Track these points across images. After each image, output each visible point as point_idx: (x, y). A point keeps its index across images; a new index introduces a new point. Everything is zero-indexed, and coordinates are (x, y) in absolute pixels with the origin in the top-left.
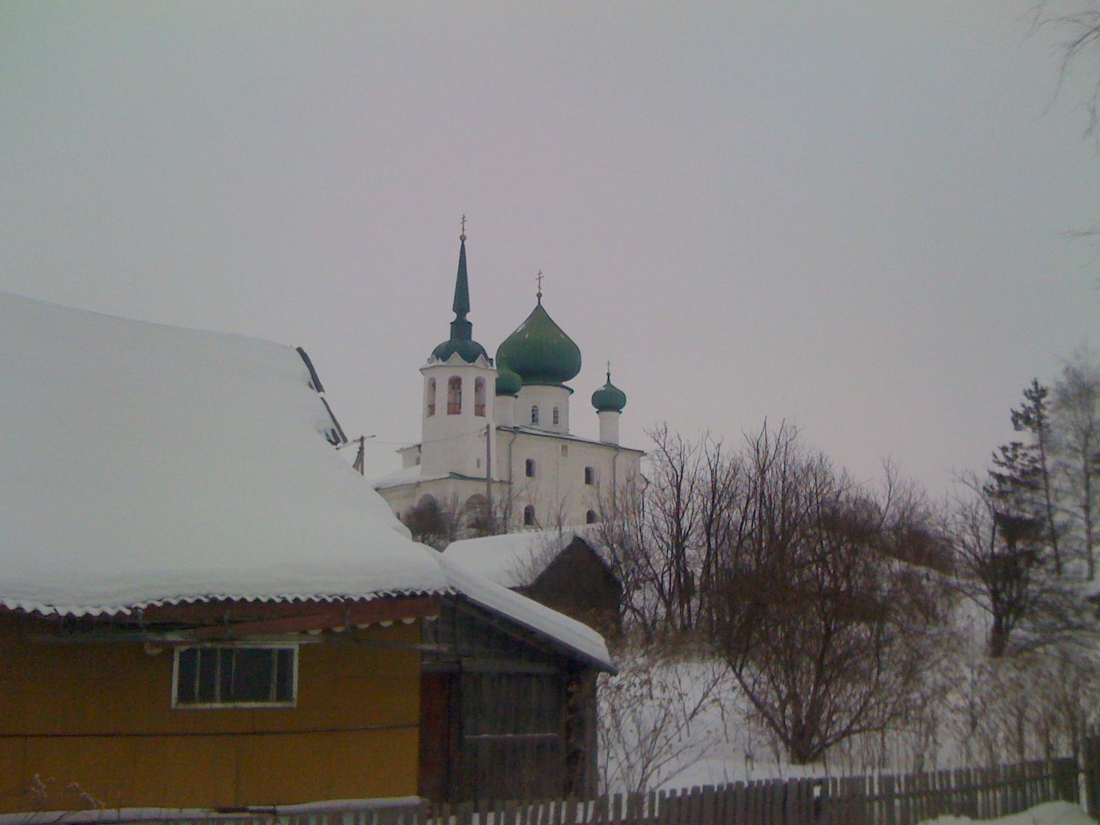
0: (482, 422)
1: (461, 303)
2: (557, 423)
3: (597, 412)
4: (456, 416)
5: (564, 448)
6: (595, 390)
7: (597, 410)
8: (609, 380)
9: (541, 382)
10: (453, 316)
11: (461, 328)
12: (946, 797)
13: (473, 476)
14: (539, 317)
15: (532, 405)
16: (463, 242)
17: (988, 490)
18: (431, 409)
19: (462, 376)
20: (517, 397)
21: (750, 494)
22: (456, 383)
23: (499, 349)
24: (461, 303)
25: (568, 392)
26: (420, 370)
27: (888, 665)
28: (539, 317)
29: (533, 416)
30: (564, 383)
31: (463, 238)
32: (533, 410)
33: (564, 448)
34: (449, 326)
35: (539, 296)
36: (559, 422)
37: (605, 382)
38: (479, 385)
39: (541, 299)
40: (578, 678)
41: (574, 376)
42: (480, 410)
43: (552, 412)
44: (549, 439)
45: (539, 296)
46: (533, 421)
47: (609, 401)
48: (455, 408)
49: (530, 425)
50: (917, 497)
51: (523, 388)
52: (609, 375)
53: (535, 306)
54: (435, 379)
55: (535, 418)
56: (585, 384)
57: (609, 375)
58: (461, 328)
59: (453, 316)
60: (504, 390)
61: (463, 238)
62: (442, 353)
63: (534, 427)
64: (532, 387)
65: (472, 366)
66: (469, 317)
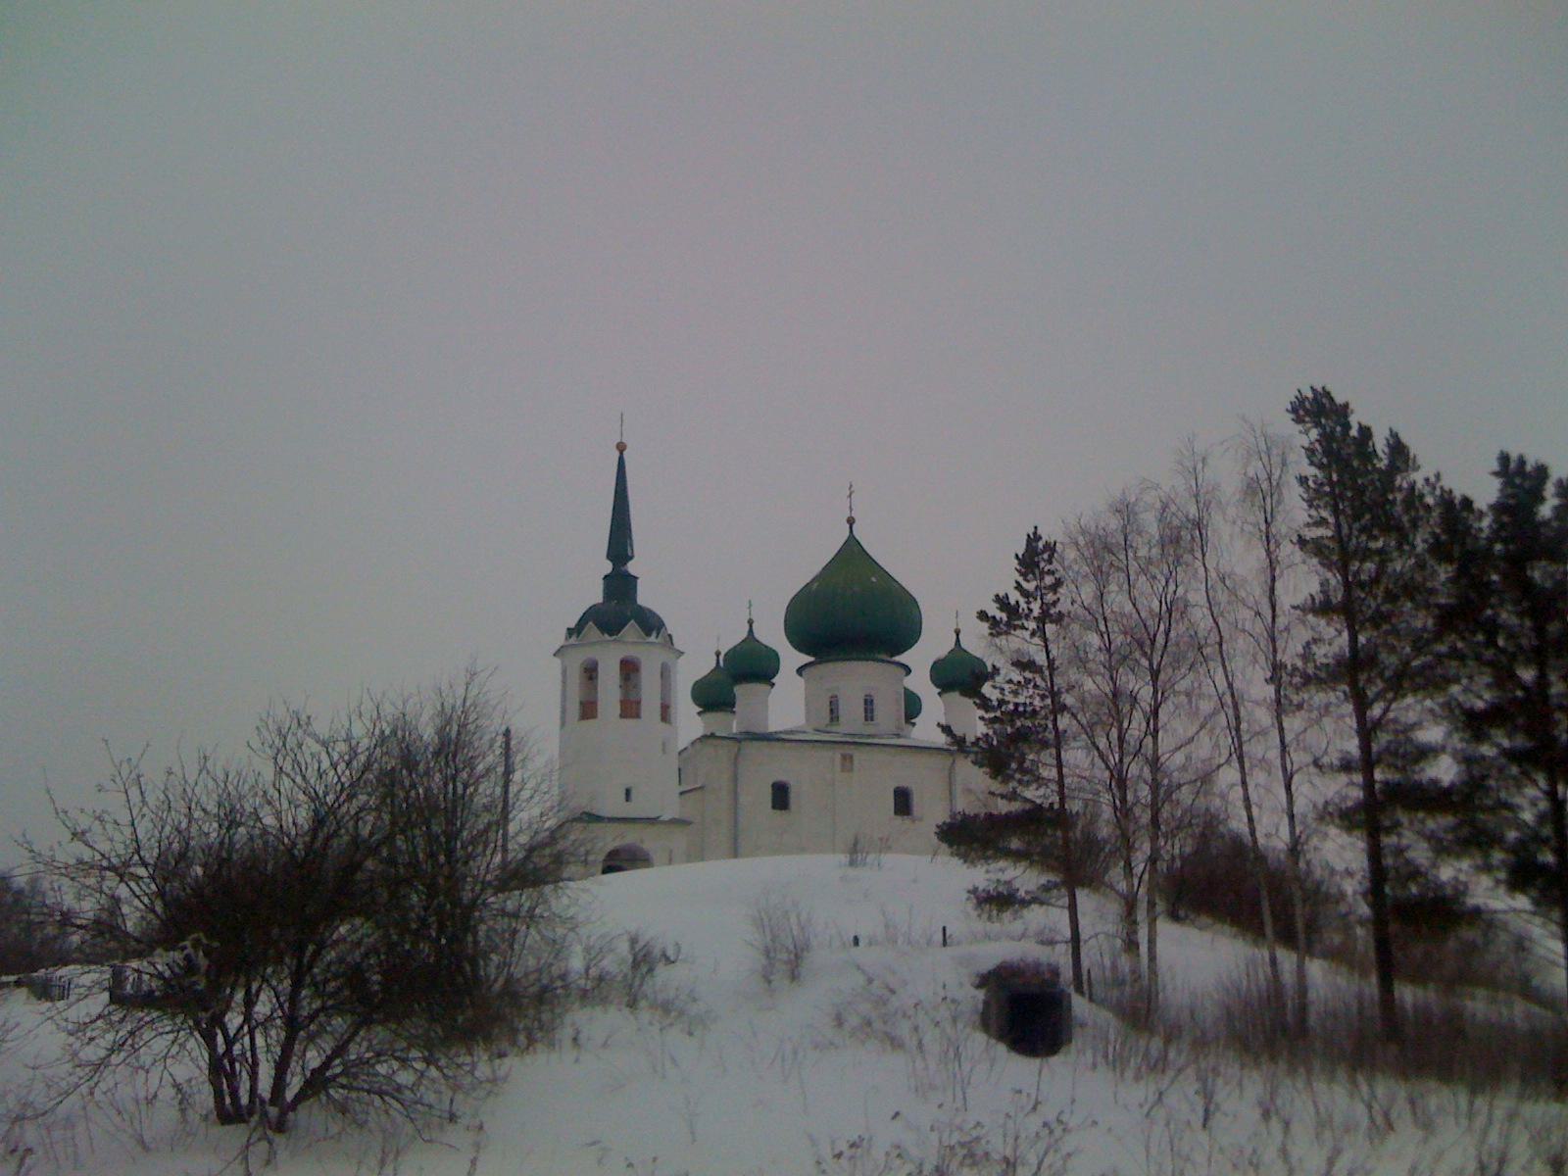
2: (872, 720)
3: (939, 694)
4: (591, 722)
5: (847, 759)
6: (931, 664)
7: (939, 690)
9: (863, 656)
10: (608, 567)
11: (620, 585)
12: (424, 1004)
13: (619, 816)
14: (852, 553)
15: (830, 695)
16: (621, 453)
18: (588, 710)
19: (597, 658)
21: (1118, 802)
23: (587, 611)
25: (904, 672)
26: (554, 655)
28: (852, 553)
29: (831, 710)
31: (621, 448)
32: (831, 702)
33: (847, 759)
34: (601, 582)
35: (851, 521)
36: (875, 717)
37: (952, 645)
39: (854, 526)
40: (82, 943)
41: (911, 647)
43: (862, 702)
44: (893, 750)
45: (851, 521)
46: (832, 719)
49: (827, 725)
52: (958, 633)
53: (845, 538)
54: (597, 664)
55: (834, 715)
57: (958, 633)
61: (621, 448)
63: (834, 729)
64: (831, 666)
65: (615, 640)
66: (632, 567)
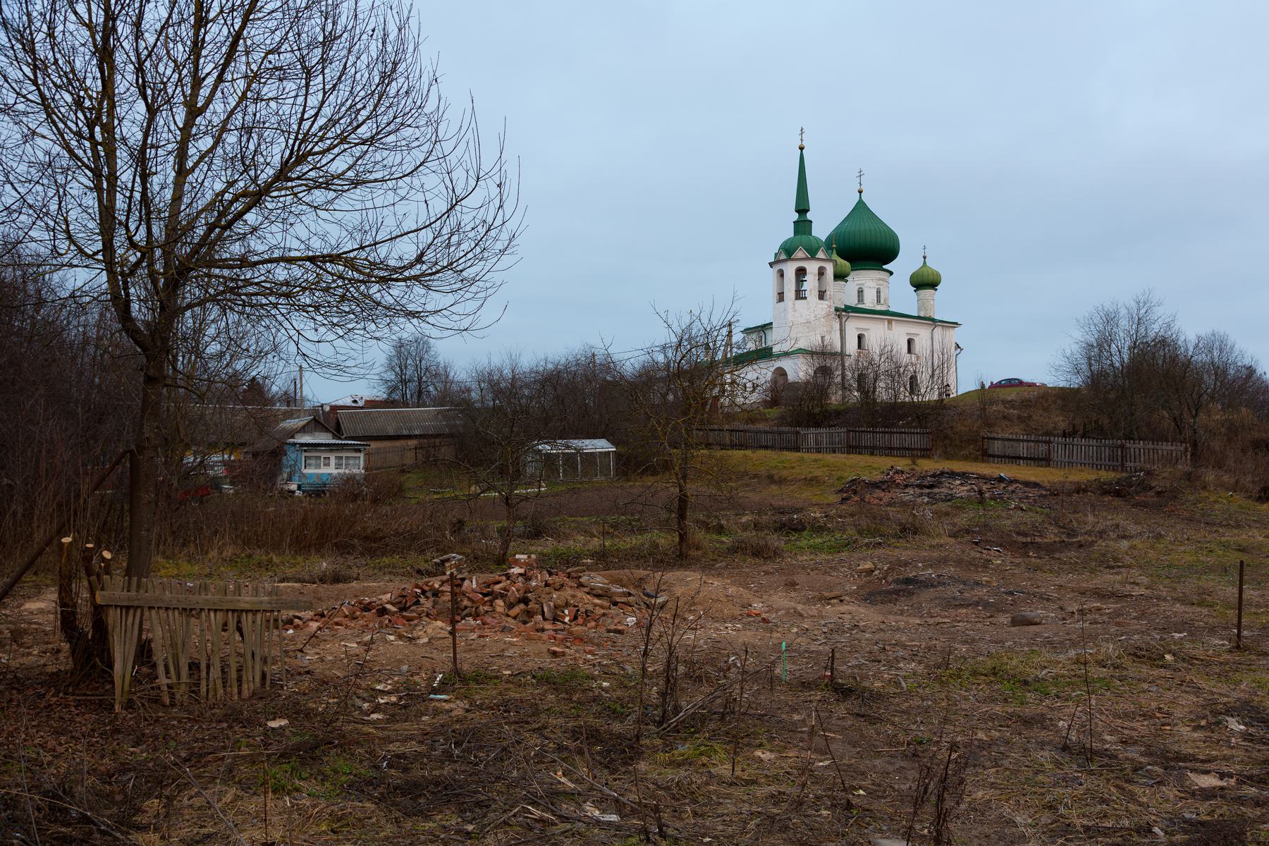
0: (824, 305)
1: (802, 209)
8: (925, 262)
11: (803, 226)
17: (586, 376)
18: (781, 297)
20: (846, 281)
22: (801, 272)
24: (802, 209)
27: (763, 538)
28: (861, 207)
30: (884, 267)
38: (821, 272)
42: (822, 295)
47: (924, 282)
48: (800, 295)
50: (480, 368)
51: (853, 274)
56: (903, 266)
58: (803, 226)
59: (809, 216)
60: (840, 276)
62: (788, 251)
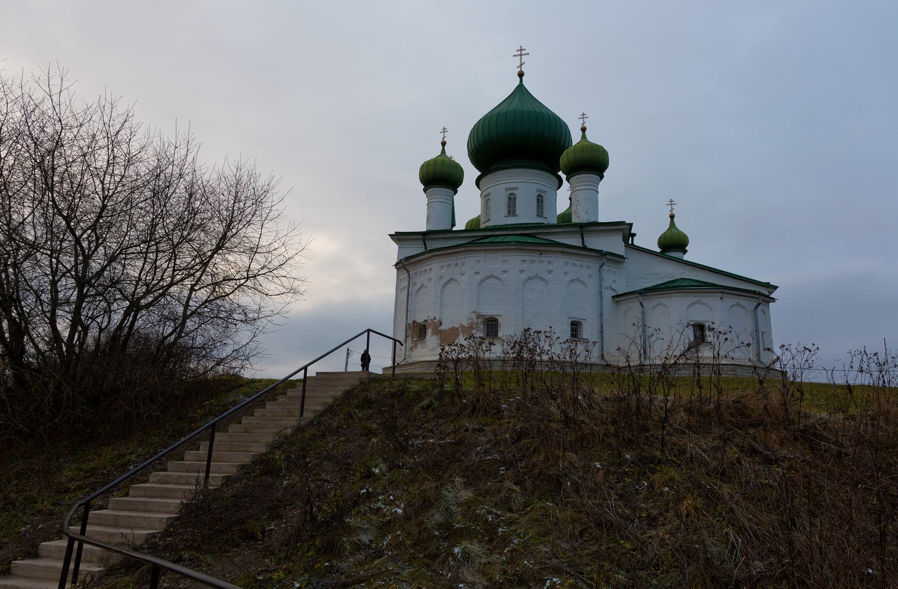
14: (521, 88)
28: (521, 88)
